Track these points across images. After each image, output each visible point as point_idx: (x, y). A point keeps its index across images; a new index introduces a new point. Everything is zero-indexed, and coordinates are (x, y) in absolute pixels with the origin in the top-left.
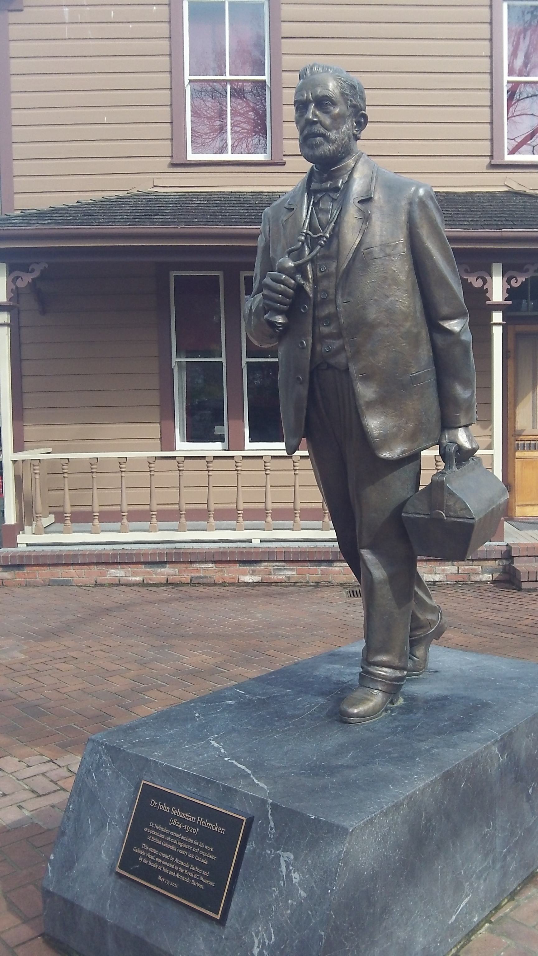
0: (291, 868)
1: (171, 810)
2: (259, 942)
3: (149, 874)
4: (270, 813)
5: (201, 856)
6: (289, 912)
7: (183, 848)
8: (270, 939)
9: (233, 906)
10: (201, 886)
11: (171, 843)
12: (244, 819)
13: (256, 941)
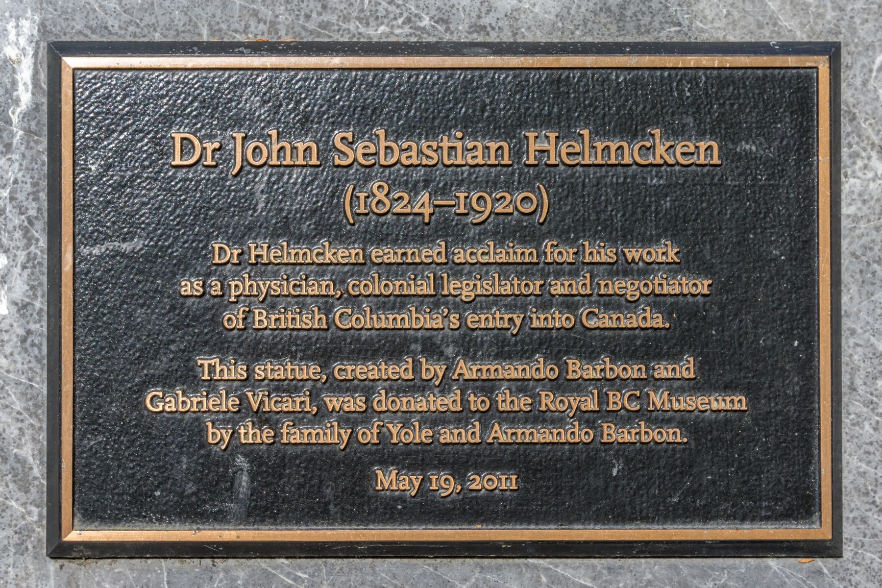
5: (611, 303)
7: (476, 304)
9: (773, 563)
10: (672, 435)
11: (399, 302)
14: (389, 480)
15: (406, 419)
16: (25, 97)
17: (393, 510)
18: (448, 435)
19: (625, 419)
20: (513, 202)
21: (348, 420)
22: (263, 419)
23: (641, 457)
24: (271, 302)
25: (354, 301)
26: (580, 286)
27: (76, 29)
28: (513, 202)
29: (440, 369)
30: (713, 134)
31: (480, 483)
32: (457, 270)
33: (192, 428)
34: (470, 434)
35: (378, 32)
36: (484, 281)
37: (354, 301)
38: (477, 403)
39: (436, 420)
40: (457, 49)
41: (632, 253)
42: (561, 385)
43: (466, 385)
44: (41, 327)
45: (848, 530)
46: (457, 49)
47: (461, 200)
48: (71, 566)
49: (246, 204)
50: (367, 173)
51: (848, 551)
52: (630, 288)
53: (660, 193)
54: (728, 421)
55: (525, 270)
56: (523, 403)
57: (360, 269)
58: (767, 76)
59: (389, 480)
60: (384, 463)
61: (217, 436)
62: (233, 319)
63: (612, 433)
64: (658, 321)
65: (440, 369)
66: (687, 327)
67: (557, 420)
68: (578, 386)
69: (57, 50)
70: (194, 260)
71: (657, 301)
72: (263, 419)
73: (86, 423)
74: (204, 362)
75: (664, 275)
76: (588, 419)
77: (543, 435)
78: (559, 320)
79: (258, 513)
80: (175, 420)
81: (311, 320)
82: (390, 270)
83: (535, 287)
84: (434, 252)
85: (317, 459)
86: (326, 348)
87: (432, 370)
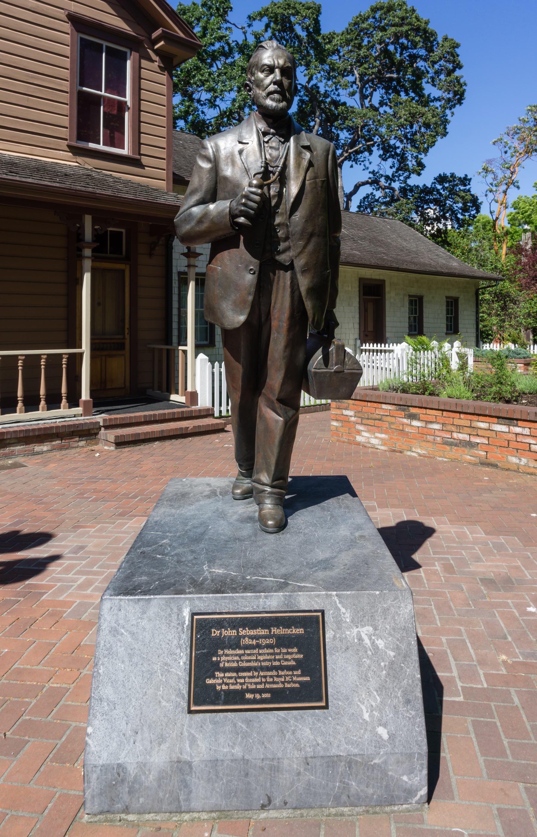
0: (373, 638)
1: (238, 632)
2: (366, 707)
3: (235, 698)
4: (338, 602)
5: (287, 660)
6: (384, 672)
7: (264, 661)
8: (375, 700)
9: (317, 711)
10: (297, 685)
11: (249, 661)
12: (123, 231)
13: (363, 708)
14: (249, 696)
15: (251, 683)
16: (187, 622)
17: (250, 702)
18: (259, 687)
19: (289, 682)
20: (268, 641)
21: (241, 684)
22: (226, 684)
23: (292, 689)
24: (228, 661)
25: (242, 661)
26: (280, 657)
27: (196, 610)
28: (268, 641)
29: (257, 674)
30: (303, 628)
31: (265, 696)
32: (260, 654)
33: (214, 686)
34: (261, 686)
35: (247, 609)
36: (264, 656)
37: (242, 661)
38: (264, 680)
39: (256, 683)
40: (260, 613)
41: (290, 650)
42: (278, 676)
43: (262, 677)
44: (188, 667)
45: (330, 704)
46: (260, 613)
47: (260, 641)
48: (191, 715)
49: (224, 642)
50: (244, 637)
51: (330, 708)
52: (289, 657)
53: (294, 639)
54: (307, 682)
55: (271, 654)
56: (271, 680)
57: (243, 655)
58: (311, 617)
59: (249, 696)
60: (247, 693)
61: (218, 688)
62: (221, 665)
63: (287, 686)
64: (294, 663)
65: (257, 674)
66: (299, 664)
67: (277, 683)
68: (281, 676)
69: (193, 614)
70: (216, 654)
71: (294, 659)
72: (226, 684)
73: (196, 686)
74: (216, 673)
75: (294, 655)
76: (283, 683)
77: (275, 686)
78: (277, 663)
79: (226, 703)
80: (211, 684)
81: (235, 665)
82: (249, 655)
83: (273, 657)
84: (256, 651)
85: (236, 691)
86: (237, 670)
87: (256, 674)
